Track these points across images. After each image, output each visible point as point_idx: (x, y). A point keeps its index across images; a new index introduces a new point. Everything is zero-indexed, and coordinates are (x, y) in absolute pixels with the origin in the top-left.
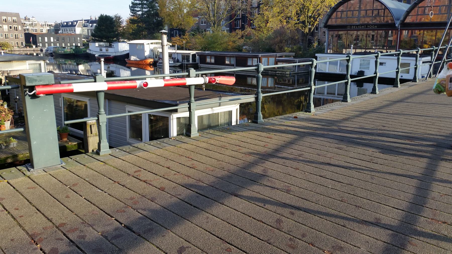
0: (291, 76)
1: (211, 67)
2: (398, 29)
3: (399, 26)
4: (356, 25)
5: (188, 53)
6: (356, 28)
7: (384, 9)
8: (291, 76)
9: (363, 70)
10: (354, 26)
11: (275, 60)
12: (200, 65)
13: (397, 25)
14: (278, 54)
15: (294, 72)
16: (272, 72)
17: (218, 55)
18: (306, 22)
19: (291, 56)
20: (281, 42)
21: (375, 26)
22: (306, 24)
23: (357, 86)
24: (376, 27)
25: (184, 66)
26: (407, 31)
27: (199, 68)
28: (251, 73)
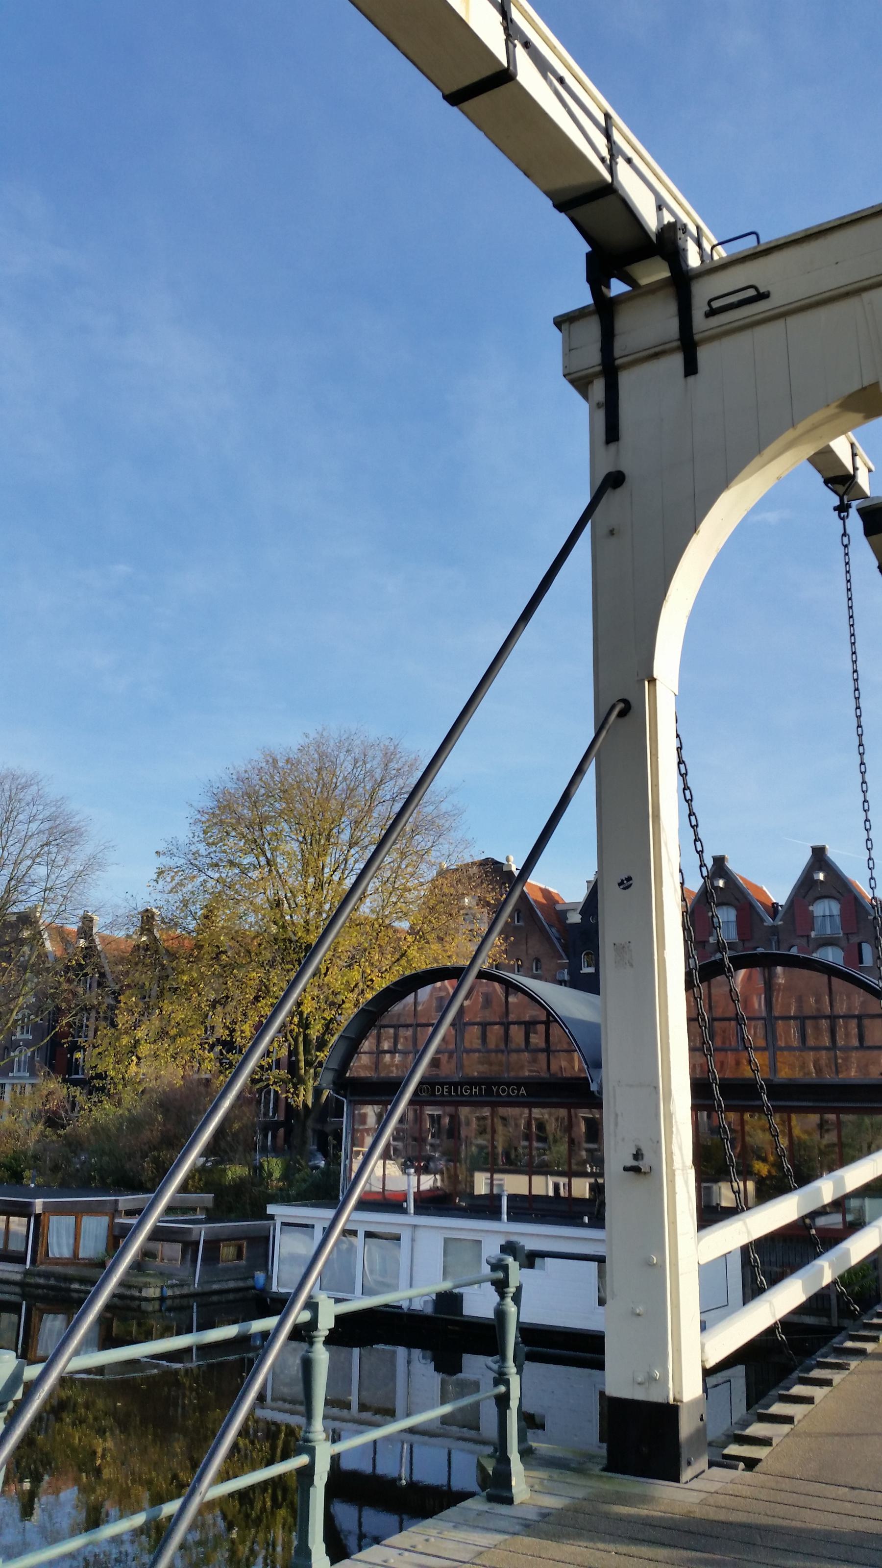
0: (170, 1309)
4: (450, 1084)
7: (547, 1023)
8: (170, 1309)
10: (442, 1084)
11: (111, 1226)
15: (185, 1291)
18: (302, 1064)
19: (194, 1210)
22: (302, 1072)
23: (437, 1369)
24: (523, 1091)
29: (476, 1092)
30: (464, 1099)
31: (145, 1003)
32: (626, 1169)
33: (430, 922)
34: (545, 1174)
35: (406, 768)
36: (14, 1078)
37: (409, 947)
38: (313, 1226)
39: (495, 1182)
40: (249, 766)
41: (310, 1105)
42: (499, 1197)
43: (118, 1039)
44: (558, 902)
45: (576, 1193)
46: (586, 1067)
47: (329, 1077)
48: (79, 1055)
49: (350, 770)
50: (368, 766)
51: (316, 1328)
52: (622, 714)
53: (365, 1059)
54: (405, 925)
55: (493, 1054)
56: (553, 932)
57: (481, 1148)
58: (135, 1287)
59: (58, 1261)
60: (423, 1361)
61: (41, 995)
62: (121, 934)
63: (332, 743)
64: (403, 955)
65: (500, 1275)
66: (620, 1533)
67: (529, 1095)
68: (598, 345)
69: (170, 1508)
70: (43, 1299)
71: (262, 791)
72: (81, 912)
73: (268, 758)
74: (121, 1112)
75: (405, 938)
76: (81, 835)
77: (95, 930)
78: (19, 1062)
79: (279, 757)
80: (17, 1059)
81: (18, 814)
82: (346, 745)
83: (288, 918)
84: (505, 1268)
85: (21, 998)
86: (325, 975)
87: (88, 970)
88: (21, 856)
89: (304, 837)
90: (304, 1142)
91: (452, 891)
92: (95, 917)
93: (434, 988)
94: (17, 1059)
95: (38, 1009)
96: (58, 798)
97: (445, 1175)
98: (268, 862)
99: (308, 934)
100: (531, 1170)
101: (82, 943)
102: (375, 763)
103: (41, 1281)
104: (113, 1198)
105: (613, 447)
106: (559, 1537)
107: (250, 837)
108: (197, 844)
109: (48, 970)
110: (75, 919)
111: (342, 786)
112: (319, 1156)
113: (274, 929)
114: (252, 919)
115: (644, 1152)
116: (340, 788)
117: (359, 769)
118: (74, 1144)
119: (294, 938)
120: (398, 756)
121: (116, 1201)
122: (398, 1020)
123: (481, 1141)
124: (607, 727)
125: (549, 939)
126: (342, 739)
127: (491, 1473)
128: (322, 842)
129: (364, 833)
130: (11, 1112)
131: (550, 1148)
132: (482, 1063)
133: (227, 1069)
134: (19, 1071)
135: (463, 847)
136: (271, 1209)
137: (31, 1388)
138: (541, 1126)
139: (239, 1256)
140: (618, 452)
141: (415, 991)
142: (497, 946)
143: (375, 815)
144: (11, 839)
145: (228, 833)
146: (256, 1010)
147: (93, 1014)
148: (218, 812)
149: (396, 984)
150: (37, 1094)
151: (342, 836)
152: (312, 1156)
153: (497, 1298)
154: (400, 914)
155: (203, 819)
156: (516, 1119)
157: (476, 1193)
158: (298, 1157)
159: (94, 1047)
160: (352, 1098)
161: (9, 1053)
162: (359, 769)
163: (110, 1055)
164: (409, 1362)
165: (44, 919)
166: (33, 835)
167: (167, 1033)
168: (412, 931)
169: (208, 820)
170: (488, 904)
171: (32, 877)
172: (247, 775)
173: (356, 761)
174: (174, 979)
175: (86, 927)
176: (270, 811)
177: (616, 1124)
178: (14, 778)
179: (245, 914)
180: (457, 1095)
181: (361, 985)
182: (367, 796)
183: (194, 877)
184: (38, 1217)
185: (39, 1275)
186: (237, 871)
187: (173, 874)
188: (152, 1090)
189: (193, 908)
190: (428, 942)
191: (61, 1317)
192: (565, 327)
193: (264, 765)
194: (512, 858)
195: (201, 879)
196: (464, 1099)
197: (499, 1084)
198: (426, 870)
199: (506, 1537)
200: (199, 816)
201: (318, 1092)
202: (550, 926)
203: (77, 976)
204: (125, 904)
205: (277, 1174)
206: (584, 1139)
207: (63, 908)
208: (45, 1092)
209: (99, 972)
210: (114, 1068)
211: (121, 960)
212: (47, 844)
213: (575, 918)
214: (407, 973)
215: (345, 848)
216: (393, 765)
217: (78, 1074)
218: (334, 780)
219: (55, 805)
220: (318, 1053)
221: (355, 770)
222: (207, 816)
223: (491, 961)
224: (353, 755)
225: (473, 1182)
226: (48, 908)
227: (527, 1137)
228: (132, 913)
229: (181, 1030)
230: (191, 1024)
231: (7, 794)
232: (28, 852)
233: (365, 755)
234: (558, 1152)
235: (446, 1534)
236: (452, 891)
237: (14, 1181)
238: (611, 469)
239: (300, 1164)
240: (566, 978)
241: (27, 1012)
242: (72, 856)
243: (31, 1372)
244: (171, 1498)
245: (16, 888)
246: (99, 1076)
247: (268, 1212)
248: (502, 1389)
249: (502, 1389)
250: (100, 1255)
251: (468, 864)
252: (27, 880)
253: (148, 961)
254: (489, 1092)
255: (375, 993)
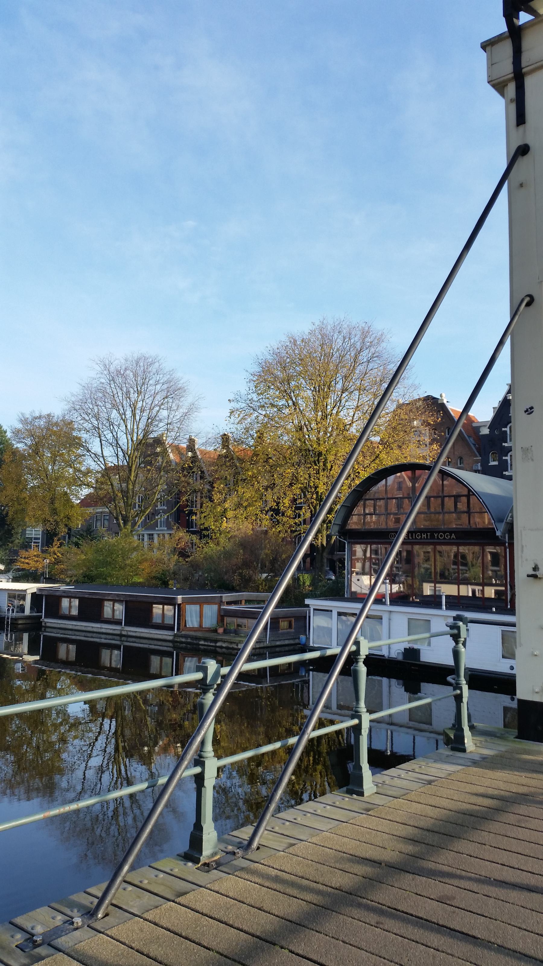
1: (71, 627)
2: (505, 543)
3: (505, 537)
5: (22, 591)
6: (413, 538)
7: (468, 496)
9: (416, 647)
11: (219, 609)
12: (46, 620)
13: (498, 533)
14: (227, 596)
16: (206, 643)
17: (86, 596)
20: (246, 564)
21: (451, 536)
23: (406, 690)
24: (453, 536)
25: (8, 622)
26: (154, 606)
27: (43, 629)
28: (160, 643)
29: (424, 537)
30: (416, 541)
31: (228, 488)
32: (528, 576)
33: (393, 436)
34: (467, 584)
35: (376, 341)
36: (158, 530)
37: (380, 452)
38: (331, 611)
39: (437, 589)
40: (280, 345)
41: (325, 545)
42: (440, 597)
43: (214, 508)
44: (474, 422)
45: (487, 595)
46: (493, 522)
47: (336, 529)
48: (194, 517)
49: (341, 344)
50: (352, 341)
51: (359, 654)
52: (528, 304)
53: (355, 519)
54: (377, 439)
55: (433, 515)
56: (471, 441)
57: (427, 569)
58: (234, 643)
59: (193, 629)
60: (397, 686)
61: (170, 485)
62: (211, 449)
63: (329, 327)
64: (377, 457)
65: (455, 631)
66: (526, 768)
67: (457, 538)
68: (511, 60)
69: (293, 740)
70: (185, 649)
71: (288, 360)
72: (188, 437)
73: (291, 339)
74: (219, 548)
75: (378, 447)
76: (185, 391)
77: (196, 447)
78: (161, 521)
79: (297, 339)
80: (159, 520)
81: (149, 380)
82: (338, 328)
83: (307, 437)
84: (458, 628)
85: (159, 486)
86: (331, 470)
87: (195, 470)
88: (153, 405)
89: (314, 388)
90: (322, 566)
91: (407, 417)
92: (195, 439)
93: (397, 476)
94: (159, 520)
95: (169, 492)
96: (171, 370)
97: (405, 585)
98: (294, 404)
99: (319, 446)
100: (459, 582)
101: (190, 454)
102: (356, 339)
103: (183, 640)
104: (220, 595)
105: (521, 128)
106: (493, 768)
107: (282, 388)
108: (252, 394)
109: (172, 470)
110: (185, 441)
111: (336, 355)
112: (331, 573)
113: (299, 444)
114: (286, 438)
115: (539, 567)
116: (335, 356)
117: (347, 343)
118: (195, 566)
119: (311, 448)
120: (371, 334)
121: (221, 596)
122: (374, 495)
123: (426, 565)
124: (519, 313)
125: (468, 445)
126: (336, 324)
127: (453, 737)
128: (326, 390)
129: (351, 383)
130: (159, 549)
131: (469, 569)
132: (426, 521)
133: (276, 525)
134: (161, 526)
135: (413, 389)
136: (307, 601)
137: (225, 678)
138: (464, 557)
139: (290, 626)
140: (525, 131)
141: (386, 478)
142: (435, 450)
143: (357, 372)
144: (146, 395)
145: (269, 387)
146: (291, 491)
147: (199, 494)
148: (263, 374)
149: (373, 474)
150: (173, 539)
151: (337, 386)
152: (327, 573)
153: (454, 644)
154: (374, 433)
155: (254, 379)
156: (448, 553)
157: (424, 594)
158: (320, 573)
159: (202, 513)
160: (350, 541)
161: (154, 517)
162: (347, 343)
163: (211, 517)
164: (390, 687)
165: (168, 441)
166: (158, 392)
167: (242, 504)
168: (382, 442)
169: (257, 380)
170: (429, 424)
171: (160, 417)
172: (278, 351)
173: (344, 338)
174: (243, 474)
175: (191, 446)
176: (293, 373)
177: (522, 551)
178: (146, 359)
179: (282, 435)
180: (413, 538)
181: (352, 476)
182: (352, 360)
183: (251, 414)
184: (179, 605)
185: (182, 636)
186: (275, 410)
187: (239, 413)
188: (235, 536)
189: (251, 433)
190: (392, 449)
191: (195, 659)
192: (488, 49)
193: (288, 344)
194: (444, 395)
195: (255, 415)
196: (416, 541)
197: (439, 532)
198: (390, 405)
199: (464, 767)
200: (252, 377)
201: (329, 537)
202: (469, 437)
203: (189, 473)
204: (213, 431)
205: (308, 583)
206: (490, 564)
207: (178, 434)
208: (177, 538)
209: (201, 471)
210: (214, 525)
211: (213, 464)
212: (167, 397)
213: (485, 431)
214: (380, 468)
215: (339, 393)
216: (367, 339)
217: (193, 528)
218: (332, 351)
219: (169, 374)
220: (328, 516)
221: (344, 344)
222: (256, 377)
223: (431, 459)
224: (342, 334)
225: (422, 588)
226: (170, 435)
227: (455, 563)
228: (217, 436)
229: (249, 503)
230: (254, 499)
231: (142, 369)
232: (157, 402)
233: (350, 334)
234: (474, 572)
235: (430, 765)
236: (407, 417)
237: (164, 586)
238: (520, 143)
239: (321, 577)
240: (480, 468)
241: (163, 494)
242: (181, 404)
243: (225, 670)
244: (294, 736)
245: (151, 424)
246: (206, 529)
247: (306, 603)
248: (458, 692)
249: (458, 692)
250: (214, 626)
251: (416, 400)
252: (157, 418)
253: (228, 464)
254: (432, 537)
255: (361, 480)
